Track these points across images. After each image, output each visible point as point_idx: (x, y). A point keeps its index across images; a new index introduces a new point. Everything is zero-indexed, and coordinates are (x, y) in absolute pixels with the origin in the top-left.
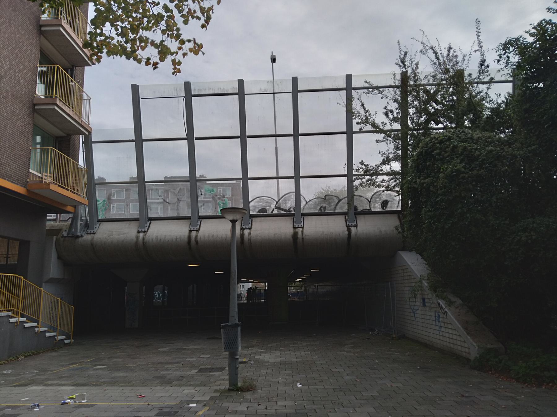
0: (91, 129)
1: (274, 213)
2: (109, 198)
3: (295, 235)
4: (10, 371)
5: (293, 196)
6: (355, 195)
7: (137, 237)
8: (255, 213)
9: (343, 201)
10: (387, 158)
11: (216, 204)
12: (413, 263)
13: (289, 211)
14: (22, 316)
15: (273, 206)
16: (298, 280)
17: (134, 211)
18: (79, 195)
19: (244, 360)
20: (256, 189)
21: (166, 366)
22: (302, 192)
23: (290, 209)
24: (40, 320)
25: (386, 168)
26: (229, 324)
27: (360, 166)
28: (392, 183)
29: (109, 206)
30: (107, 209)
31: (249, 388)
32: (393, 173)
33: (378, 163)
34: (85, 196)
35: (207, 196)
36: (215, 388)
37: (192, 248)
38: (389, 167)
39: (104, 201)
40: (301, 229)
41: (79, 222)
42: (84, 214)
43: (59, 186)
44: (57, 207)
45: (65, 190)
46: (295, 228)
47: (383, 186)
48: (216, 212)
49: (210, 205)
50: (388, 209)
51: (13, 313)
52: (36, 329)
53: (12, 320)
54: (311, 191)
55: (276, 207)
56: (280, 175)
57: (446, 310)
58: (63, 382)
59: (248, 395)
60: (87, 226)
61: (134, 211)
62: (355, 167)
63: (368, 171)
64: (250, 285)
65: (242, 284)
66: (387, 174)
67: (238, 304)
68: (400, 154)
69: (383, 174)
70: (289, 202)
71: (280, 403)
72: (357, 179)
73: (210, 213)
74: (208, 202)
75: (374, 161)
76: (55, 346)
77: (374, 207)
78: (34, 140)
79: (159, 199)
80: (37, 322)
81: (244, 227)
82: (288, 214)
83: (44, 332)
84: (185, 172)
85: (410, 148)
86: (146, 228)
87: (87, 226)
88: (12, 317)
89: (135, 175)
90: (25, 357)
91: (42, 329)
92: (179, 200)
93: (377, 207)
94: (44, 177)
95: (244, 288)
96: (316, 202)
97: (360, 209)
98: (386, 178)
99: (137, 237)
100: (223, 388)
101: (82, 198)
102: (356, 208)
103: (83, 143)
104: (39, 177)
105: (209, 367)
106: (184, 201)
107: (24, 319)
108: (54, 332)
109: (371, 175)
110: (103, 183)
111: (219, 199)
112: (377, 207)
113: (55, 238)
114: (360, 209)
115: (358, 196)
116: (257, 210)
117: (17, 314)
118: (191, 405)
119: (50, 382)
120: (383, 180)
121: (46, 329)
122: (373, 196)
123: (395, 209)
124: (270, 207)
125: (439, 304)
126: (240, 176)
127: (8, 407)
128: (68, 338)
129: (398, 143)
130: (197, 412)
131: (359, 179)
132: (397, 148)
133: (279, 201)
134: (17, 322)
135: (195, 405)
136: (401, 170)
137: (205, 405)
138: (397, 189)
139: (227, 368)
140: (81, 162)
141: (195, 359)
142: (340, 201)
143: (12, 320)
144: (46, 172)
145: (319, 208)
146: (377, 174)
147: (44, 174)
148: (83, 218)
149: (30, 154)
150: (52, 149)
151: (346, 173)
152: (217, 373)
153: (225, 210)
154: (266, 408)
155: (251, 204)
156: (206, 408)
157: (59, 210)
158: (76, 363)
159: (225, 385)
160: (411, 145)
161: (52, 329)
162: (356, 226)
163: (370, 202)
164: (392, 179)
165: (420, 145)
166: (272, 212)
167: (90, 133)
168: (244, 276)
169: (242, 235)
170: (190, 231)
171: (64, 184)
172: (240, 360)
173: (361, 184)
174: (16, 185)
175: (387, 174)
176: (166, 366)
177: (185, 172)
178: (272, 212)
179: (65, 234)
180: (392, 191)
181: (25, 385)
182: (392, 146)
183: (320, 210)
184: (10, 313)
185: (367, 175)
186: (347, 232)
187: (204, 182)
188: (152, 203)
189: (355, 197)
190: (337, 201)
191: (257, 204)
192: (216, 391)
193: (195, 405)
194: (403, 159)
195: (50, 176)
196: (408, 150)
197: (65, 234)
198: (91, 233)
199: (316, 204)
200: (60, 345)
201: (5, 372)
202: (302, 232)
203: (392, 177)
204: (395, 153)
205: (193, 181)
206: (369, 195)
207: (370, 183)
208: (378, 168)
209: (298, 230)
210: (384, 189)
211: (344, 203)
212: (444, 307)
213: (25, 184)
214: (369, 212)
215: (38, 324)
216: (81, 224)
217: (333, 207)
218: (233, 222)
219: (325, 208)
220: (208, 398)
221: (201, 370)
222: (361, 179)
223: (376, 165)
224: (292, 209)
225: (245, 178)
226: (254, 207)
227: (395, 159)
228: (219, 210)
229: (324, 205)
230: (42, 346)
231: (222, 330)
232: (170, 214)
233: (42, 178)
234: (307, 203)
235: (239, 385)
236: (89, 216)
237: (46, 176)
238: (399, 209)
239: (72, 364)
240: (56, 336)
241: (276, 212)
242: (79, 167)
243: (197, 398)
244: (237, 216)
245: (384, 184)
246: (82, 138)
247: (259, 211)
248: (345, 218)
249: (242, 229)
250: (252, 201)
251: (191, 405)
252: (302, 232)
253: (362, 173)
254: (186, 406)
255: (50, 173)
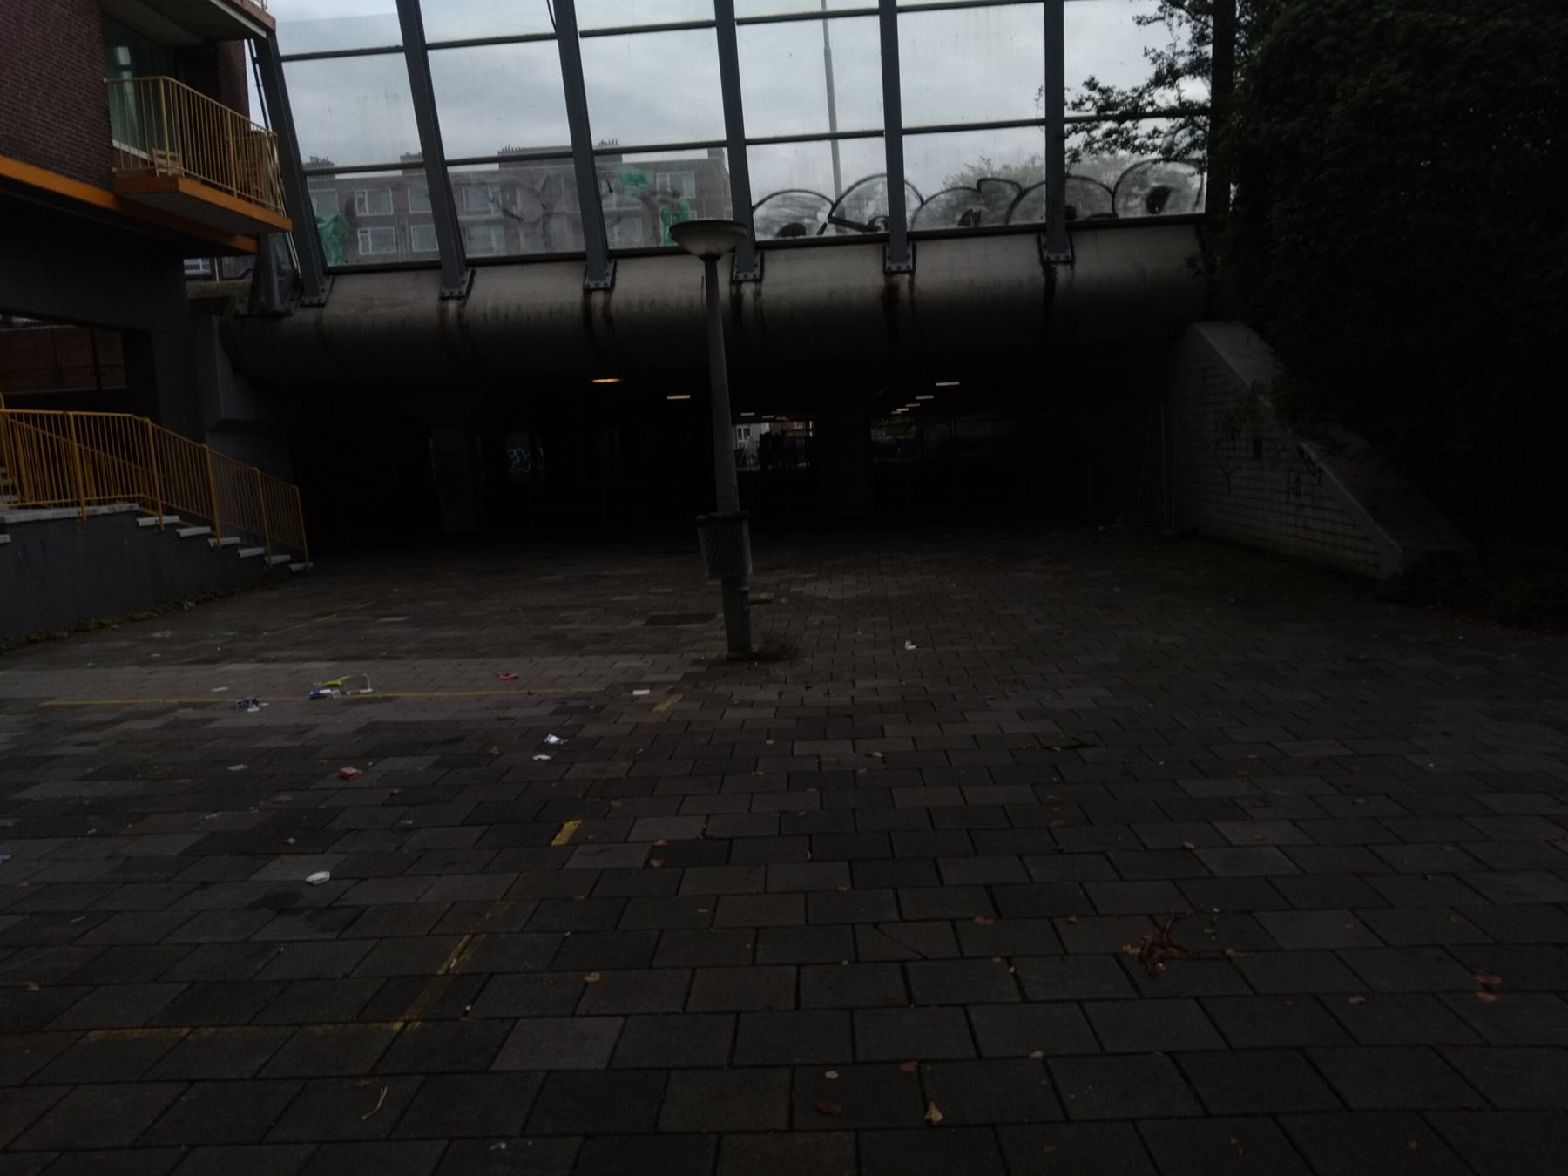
0: (274, 21)
1: (826, 234)
2: (349, 211)
3: (890, 293)
4: (168, 634)
5: (882, 187)
6: (1069, 176)
7: (443, 312)
8: (769, 238)
9: (1033, 194)
10: (1171, 66)
11: (655, 216)
12: (1236, 353)
13: (872, 226)
14: (169, 512)
15: (823, 217)
16: (900, 410)
17: (423, 243)
18: (263, 206)
19: (763, 596)
20: (768, 172)
21: (563, 614)
22: (908, 174)
23: (872, 221)
24: (217, 521)
25: (1165, 97)
26: (719, 514)
27: (1086, 92)
28: (1183, 138)
29: (353, 233)
30: (350, 242)
31: (781, 653)
32: (1185, 110)
33: (1141, 83)
34: (281, 206)
35: (627, 197)
36: (693, 656)
37: (596, 334)
38: (1175, 92)
39: (336, 219)
40: (907, 277)
41: (276, 279)
42: (286, 255)
43: (204, 183)
44: (212, 234)
45: (223, 195)
46: (888, 274)
47: (1155, 148)
48: (656, 236)
49: (638, 223)
50: (1168, 212)
51: (143, 505)
52: (212, 542)
53: (143, 522)
54: (934, 169)
55: (831, 219)
56: (842, 127)
57: (1321, 464)
58: (305, 654)
59: (779, 670)
60: (299, 287)
61: (423, 243)
62: (1070, 97)
63: (1109, 105)
64: (766, 428)
65: (743, 427)
66: (1169, 113)
67: (738, 474)
68: (1210, 55)
69: (1158, 114)
70: (871, 203)
71: (860, 684)
72: (1075, 130)
73: (638, 240)
74: (630, 215)
75: (1127, 77)
76: (264, 578)
77: (1126, 208)
78: (112, 59)
79: (489, 212)
80: (211, 524)
81: (741, 277)
82: (868, 237)
83: (234, 547)
84: (558, 135)
85: (1240, 37)
86: (464, 289)
87: (299, 287)
88: (143, 515)
89: (414, 147)
90: (198, 603)
91: (225, 541)
92: (548, 216)
93: (1135, 208)
94: (159, 161)
95: (751, 435)
96: (948, 202)
97: (1083, 213)
98: (1164, 124)
99: (443, 312)
100: (714, 656)
101: (273, 213)
102: (1071, 212)
103: (254, 61)
104: (144, 161)
105: (675, 612)
106: (560, 214)
107: (175, 519)
108: (258, 545)
109: (1120, 119)
110: (325, 171)
111: (663, 202)
112: (1135, 208)
113: (215, 320)
114: (1083, 213)
115: (1076, 177)
116: (776, 230)
117: (154, 507)
118: (636, 693)
119: (271, 655)
120: (1156, 132)
121: (236, 540)
122: (1122, 177)
123: (1188, 211)
124: (815, 218)
125: (1301, 451)
126: (722, 136)
127: (186, 705)
128: (297, 557)
129: (1205, 23)
130: (654, 705)
131: (1083, 129)
132: (1200, 39)
133: (840, 200)
134: (157, 526)
135: (646, 692)
136: (1212, 101)
137: (671, 692)
138: (1197, 154)
139: (721, 615)
140: (257, 116)
141: (635, 598)
142: (1023, 193)
143: (143, 522)
144: (162, 147)
145: (959, 217)
146: (1136, 114)
147: (157, 152)
148: (286, 267)
149: (106, 95)
150: (166, 82)
151: (1042, 114)
152: (695, 626)
153: (682, 230)
154: (828, 694)
155: (759, 213)
156: (676, 699)
157: (212, 250)
158: (328, 614)
159: (721, 649)
160: (1245, 28)
161: (252, 539)
162: (1070, 262)
163: (1113, 194)
164: (1182, 127)
165: (1276, 24)
166: (821, 232)
167: (271, 32)
168: (751, 402)
169: (737, 299)
170: (588, 292)
171: (216, 174)
172: (752, 596)
173: (1088, 145)
174: (82, 186)
175: (1169, 113)
176: (563, 614)
177: (558, 135)
178: (821, 232)
179: (242, 309)
180: (1183, 161)
181: (214, 661)
182: (1185, 32)
183: (962, 222)
184: (136, 506)
185: (1107, 118)
186: (1042, 280)
187: (325, 179)
188: (473, 224)
189: (1069, 183)
190: (1014, 195)
191: (773, 213)
192: (696, 662)
193: (646, 692)
194: (1217, 70)
195: (173, 158)
196: (1236, 41)
197: (242, 309)
198: (311, 305)
199: (951, 208)
200: (281, 575)
201: (158, 635)
202: (911, 283)
203: (1182, 120)
204: (1193, 53)
205: (585, 158)
206: (1111, 178)
207: (1115, 142)
208: (1141, 96)
209: (896, 279)
210: (1155, 155)
211: (1034, 201)
212: (1314, 457)
213: (104, 181)
214: (1109, 223)
215: (213, 528)
216: (280, 283)
217: (1002, 212)
218: (710, 260)
219: (981, 208)
220: (678, 677)
221: (652, 621)
222: (1089, 131)
223: (1135, 90)
224: (879, 223)
225: (736, 141)
226: (766, 220)
227: (1195, 68)
228: (665, 233)
229: (975, 208)
230: (225, 581)
231: (700, 532)
232: (525, 247)
233: (152, 164)
234: (923, 203)
235: (755, 647)
236: (301, 261)
237: (161, 157)
238: (1201, 210)
239: (320, 615)
240: (266, 554)
241: (831, 232)
242: (253, 128)
243: (647, 679)
244: (720, 245)
245: (1158, 141)
246: (248, 49)
247: (784, 232)
248: (1039, 241)
249: (736, 283)
250: (760, 203)
251: (636, 693)
252: (911, 283)
253: (1093, 113)
254: (626, 694)
255: (172, 149)
